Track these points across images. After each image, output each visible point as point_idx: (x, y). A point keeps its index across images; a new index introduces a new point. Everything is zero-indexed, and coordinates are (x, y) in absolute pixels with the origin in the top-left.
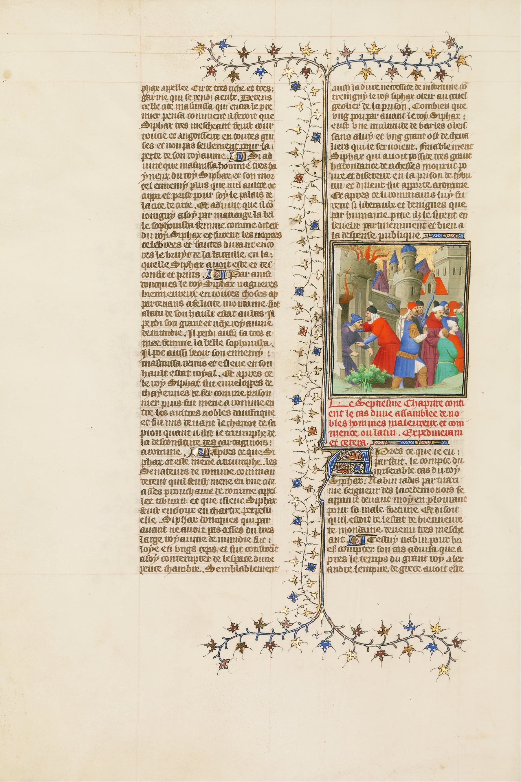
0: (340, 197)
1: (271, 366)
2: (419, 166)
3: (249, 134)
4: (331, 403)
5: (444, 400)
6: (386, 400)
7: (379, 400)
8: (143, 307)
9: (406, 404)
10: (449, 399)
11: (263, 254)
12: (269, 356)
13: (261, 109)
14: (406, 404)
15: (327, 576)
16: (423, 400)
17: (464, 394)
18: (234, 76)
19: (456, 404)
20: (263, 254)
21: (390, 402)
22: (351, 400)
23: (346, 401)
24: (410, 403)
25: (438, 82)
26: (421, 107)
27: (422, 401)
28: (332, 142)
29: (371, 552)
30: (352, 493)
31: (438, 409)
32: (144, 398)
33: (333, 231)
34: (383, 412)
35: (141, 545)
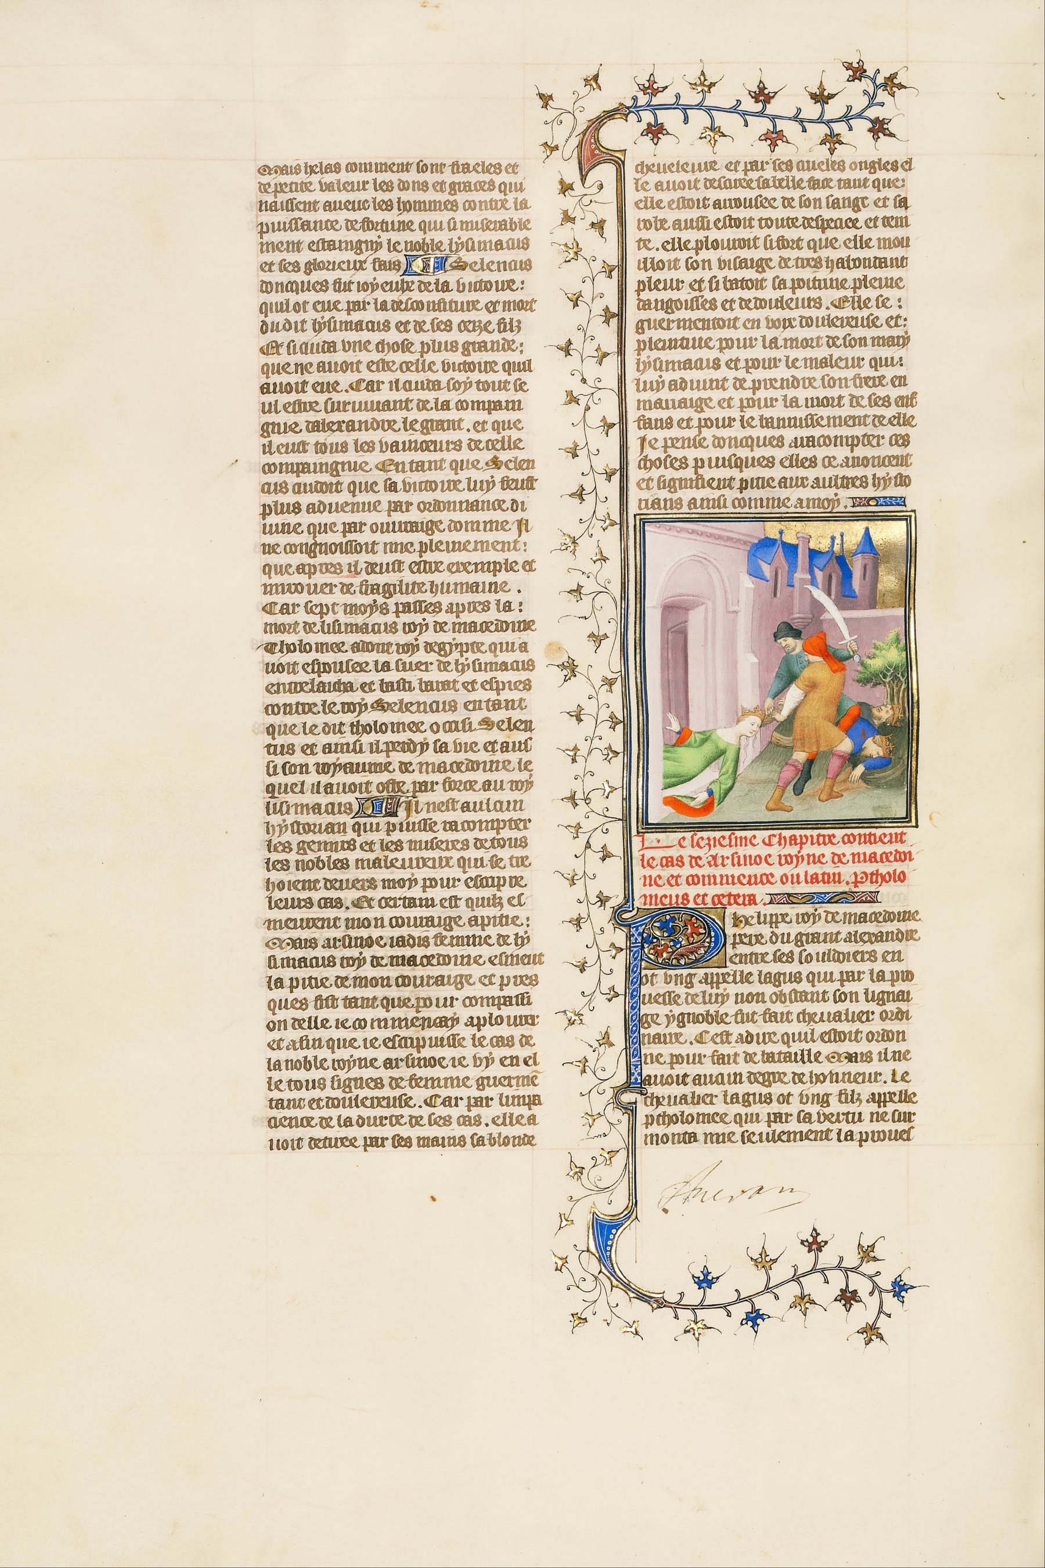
4: (643, 841)
5: (839, 833)
6: (727, 834)
8: (264, 515)
9: (767, 841)
10: (849, 831)
14: (767, 841)
15: (647, 1154)
16: (798, 833)
17: (909, 818)
18: (832, 140)
19: (862, 840)
21: (736, 838)
22: (680, 835)
23: (674, 837)
24: (775, 840)
31: (828, 850)
32: (904, 470)
35: (269, 855)
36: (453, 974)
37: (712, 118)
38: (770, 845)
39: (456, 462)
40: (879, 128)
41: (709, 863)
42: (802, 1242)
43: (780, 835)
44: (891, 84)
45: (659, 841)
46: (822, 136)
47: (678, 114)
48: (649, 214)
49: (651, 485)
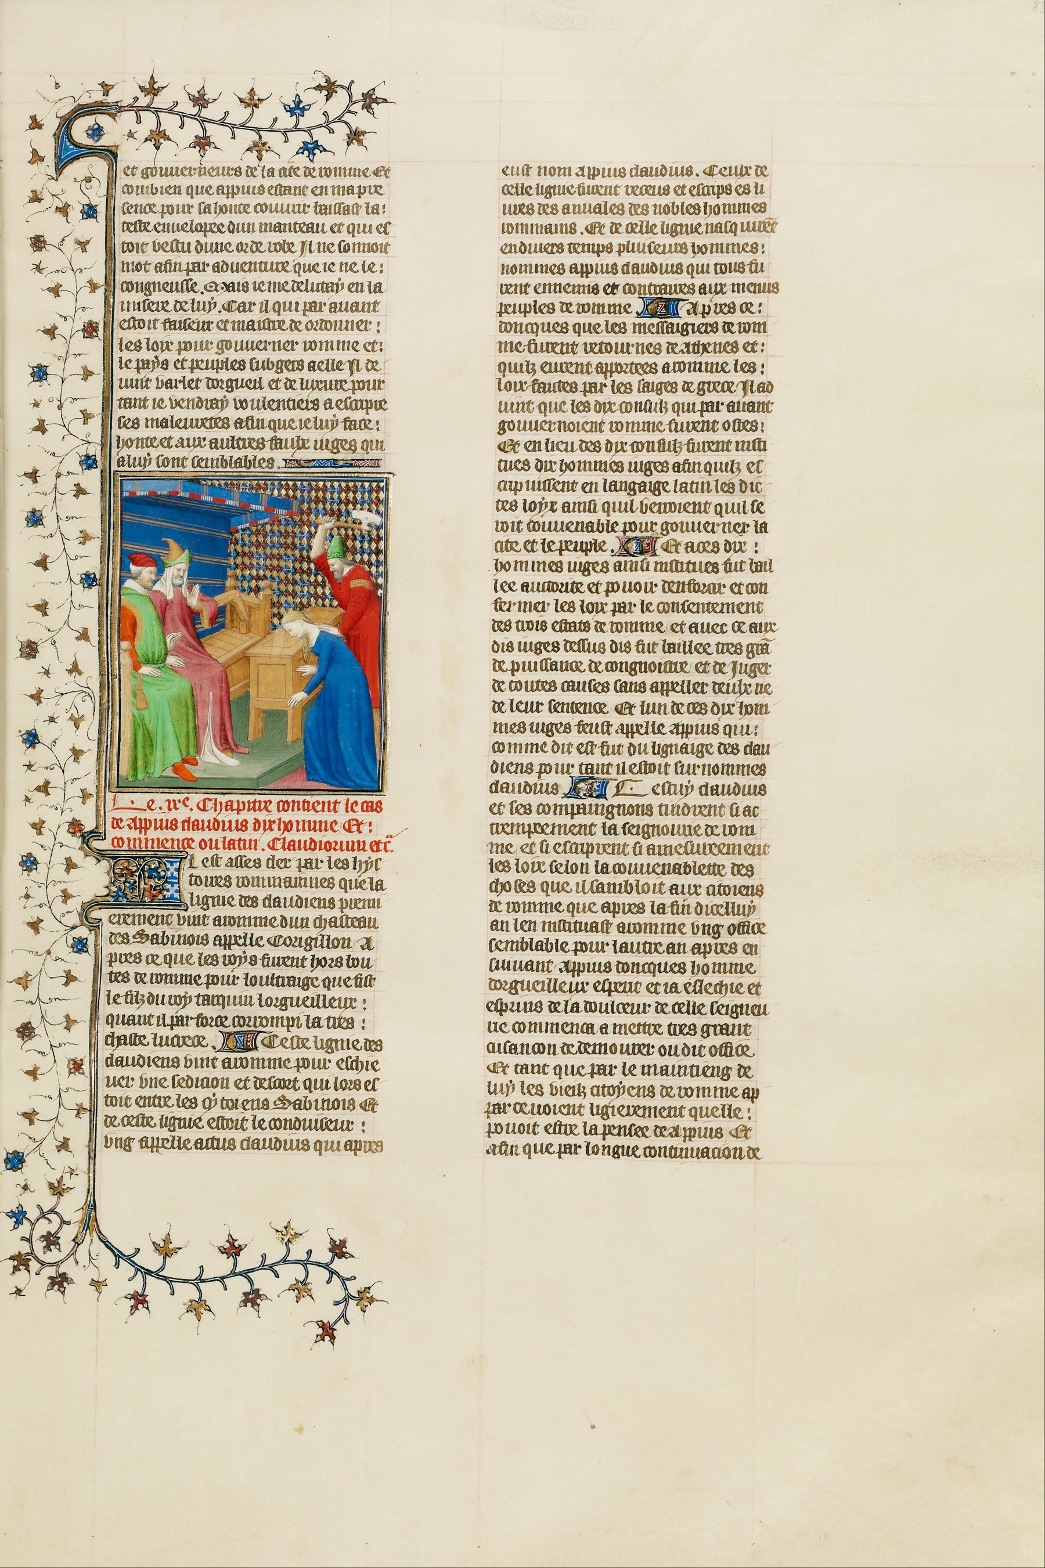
0: (631, 713)
1: (753, 833)
2: (541, 1007)
3: (538, 682)
7: (308, 798)
9: (201, 806)
10: (284, 798)
11: (608, 485)
12: (370, 831)
13: (513, 671)
15: (103, 1154)
18: (259, 148)
20: (608, 485)
25: (303, 160)
26: (284, 943)
27: (232, 802)
28: (120, 354)
29: (648, 1054)
30: (727, 1014)
33: (120, 354)
34: (552, 1032)
36: (324, 840)
37: (204, 129)
38: (204, 810)
39: (274, 421)
40: (355, 136)
41: (129, 825)
42: (374, 89)
43: (216, 800)
44: (370, 100)
45: (133, 802)
46: (250, 144)
47: (280, 136)
48: (132, 218)
49: (248, 1085)
